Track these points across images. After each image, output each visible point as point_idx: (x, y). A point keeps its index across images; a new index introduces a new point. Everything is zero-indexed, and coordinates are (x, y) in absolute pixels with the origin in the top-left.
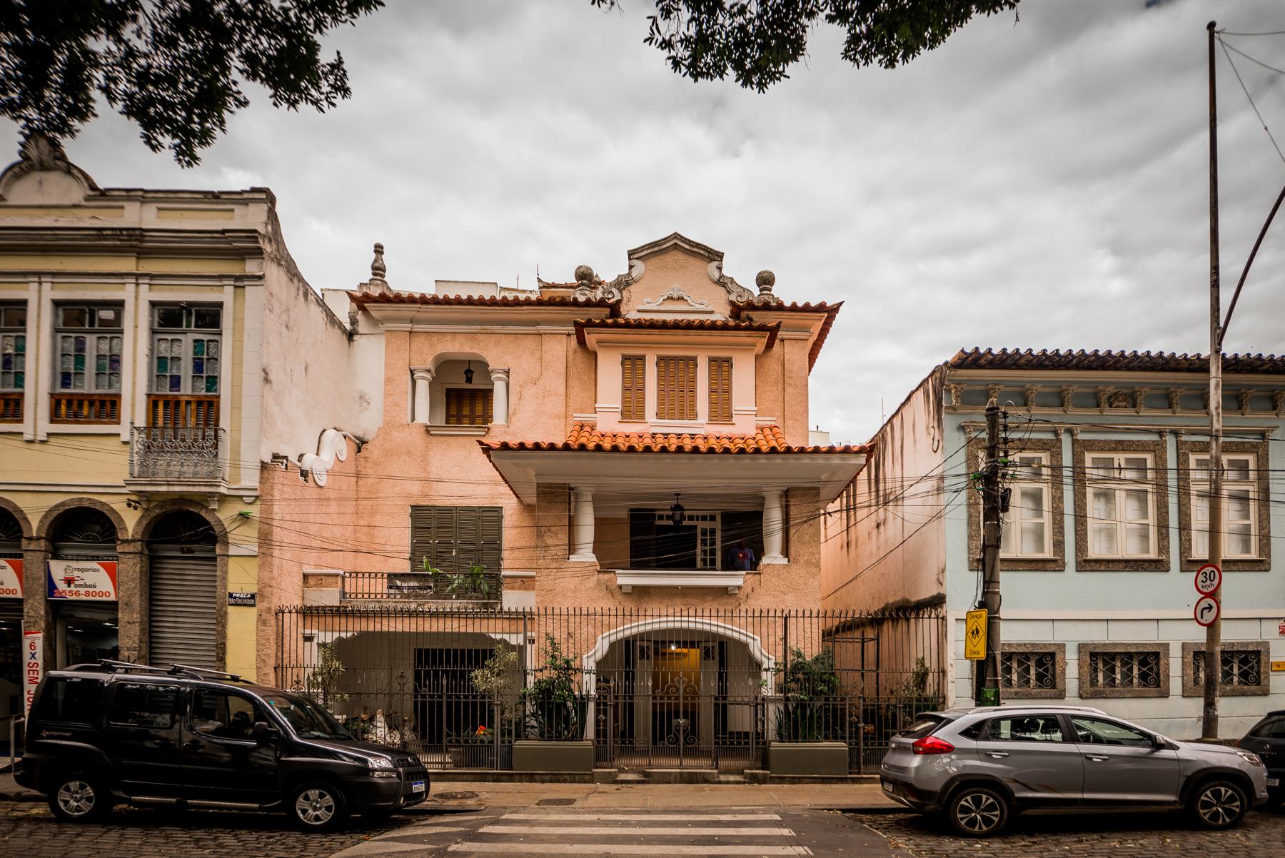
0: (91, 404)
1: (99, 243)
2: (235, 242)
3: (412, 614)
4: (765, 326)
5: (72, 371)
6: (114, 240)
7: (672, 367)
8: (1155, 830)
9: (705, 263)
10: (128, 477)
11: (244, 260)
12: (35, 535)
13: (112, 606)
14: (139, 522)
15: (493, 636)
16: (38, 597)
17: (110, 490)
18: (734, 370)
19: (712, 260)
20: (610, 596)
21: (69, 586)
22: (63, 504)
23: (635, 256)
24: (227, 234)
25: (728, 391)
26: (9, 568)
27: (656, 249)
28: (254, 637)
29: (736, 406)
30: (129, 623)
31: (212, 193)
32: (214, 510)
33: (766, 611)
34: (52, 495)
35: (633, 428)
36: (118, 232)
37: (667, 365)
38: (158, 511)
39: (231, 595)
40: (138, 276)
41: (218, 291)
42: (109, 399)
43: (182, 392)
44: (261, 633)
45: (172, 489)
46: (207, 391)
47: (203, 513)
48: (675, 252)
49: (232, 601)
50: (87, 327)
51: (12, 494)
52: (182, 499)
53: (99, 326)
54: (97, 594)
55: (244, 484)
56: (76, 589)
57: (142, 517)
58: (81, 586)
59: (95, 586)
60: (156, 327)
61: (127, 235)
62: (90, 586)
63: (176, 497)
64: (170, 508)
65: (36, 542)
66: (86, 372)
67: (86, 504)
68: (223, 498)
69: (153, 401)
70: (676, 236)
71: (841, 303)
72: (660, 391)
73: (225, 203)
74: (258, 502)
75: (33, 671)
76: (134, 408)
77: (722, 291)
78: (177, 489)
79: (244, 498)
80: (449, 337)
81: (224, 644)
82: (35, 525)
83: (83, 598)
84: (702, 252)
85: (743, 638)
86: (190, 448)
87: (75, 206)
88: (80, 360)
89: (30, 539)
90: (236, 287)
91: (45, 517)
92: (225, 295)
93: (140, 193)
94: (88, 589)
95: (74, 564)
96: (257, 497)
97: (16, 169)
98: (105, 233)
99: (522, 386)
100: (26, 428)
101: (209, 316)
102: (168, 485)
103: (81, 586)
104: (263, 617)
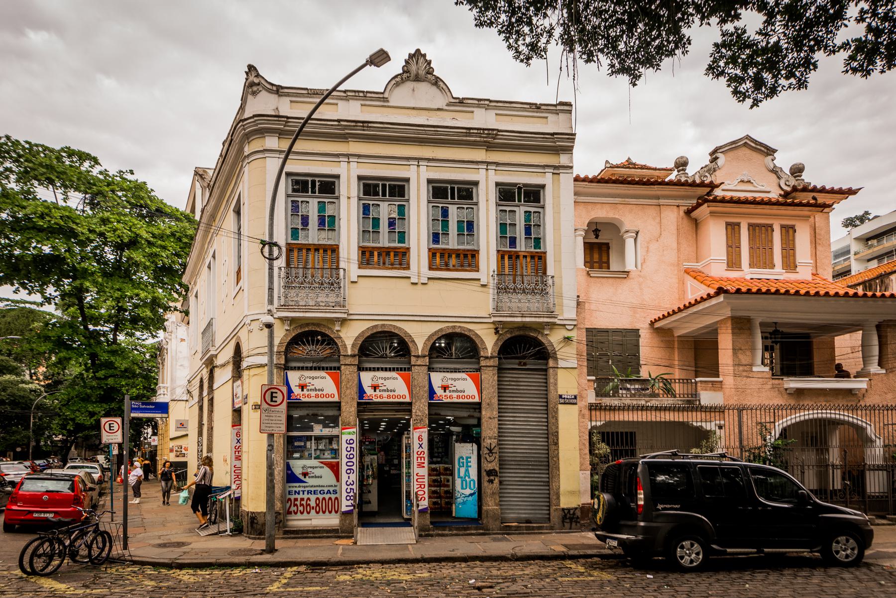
0: (458, 256)
2: (559, 141)
3: (643, 408)
4: (825, 204)
6: (476, 137)
7: (757, 231)
8: (806, 567)
9: (763, 157)
10: (491, 311)
11: (559, 154)
13: (477, 406)
14: (496, 344)
15: (695, 424)
16: (423, 401)
17: (477, 320)
18: (797, 234)
19: (768, 155)
20: (780, 396)
21: (445, 392)
22: (441, 330)
23: (721, 151)
25: (793, 249)
26: (328, 377)
27: (734, 146)
29: (799, 259)
30: (490, 418)
31: (536, 104)
32: (547, 335)
35: (733, 275)
37: (754, 230)
38: (509, 336)
39: (560, 396)
40: (488, 163)
43: (518, 249)
44: (581, 424)
45: (525, 319)
46: (535, 248)
47: (540, 337)
48: (744, 148)
49: (562, 401)
50: (517, 202)
51: (399, 322)
52: (524, 327)
55: (566, 316)
57: (498, 339)
59: (464, 392)
61: (487, 134)
63: (521, 325)
64: (517, 333)
65: (422, 359)
67: (458, 330)
69: (501, 255)
70: (748, 137)
71: (860, 189)
72: (751, 248)
73: (542, 112)
74: (575, 330)
76: (488, 261)
77: (774, 176)
78: (528, 319)
79: (567, 327)
80: (599, 206)
81: (557, 432)
82: (420, 346)
83: (455, 400)
84: (763, 149)
85: (864, 425)
87: (439, 109)
88: (445, 224)
89: (418, 357)
90: (553, 173)
92: (547, 179)
94: (459, 394)
95: (449, 375)
96: (575, 325)
97: (398, 79)
98: (472, 131)
99: (648, 243)
100: (413, 272)
101: (533, 194)
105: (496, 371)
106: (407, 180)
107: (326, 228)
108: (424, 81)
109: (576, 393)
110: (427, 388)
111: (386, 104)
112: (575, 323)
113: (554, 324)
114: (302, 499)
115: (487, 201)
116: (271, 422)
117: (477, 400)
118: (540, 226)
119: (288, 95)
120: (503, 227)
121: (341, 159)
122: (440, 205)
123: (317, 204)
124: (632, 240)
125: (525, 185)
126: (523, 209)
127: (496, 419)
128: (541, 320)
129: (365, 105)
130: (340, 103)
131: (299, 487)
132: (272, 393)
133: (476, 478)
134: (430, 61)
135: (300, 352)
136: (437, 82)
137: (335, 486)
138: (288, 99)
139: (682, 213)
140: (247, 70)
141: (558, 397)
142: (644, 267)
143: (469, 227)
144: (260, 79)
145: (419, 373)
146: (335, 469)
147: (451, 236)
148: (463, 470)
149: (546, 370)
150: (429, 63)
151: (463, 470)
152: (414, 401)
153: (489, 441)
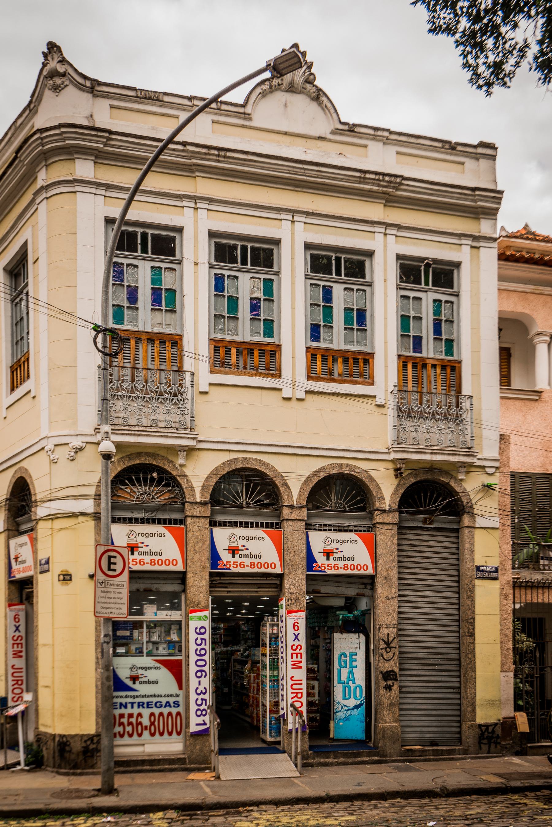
1: (357, 185)
2: (481, 201)
5: (322, 323)
6: (373, 184)
12: (295, 503)
16: (299, 572)
22: (323, 469)
24: (477, 193)
28: (498, 612)
30: (388, 598)
32: (461, 480)
33: (114, 562)
34: (312, 459)
36: (381, 178)
38: (413, 480)
39: (478, 568)
42: (363, 357)
44: (504, 607)
47: (453, 484)
49: (480, 575)
54: (164, 562)
56: (242, 560)
57: (398, 485)
60: (309, 273)
61: (388, 182)
62: (156, 554)
63: (428, 466)
64: (423, 477)
66: (334, 324)
67: (346, 470)
68: (468, 467)
69: (403, 361)
75: (297, 654)
78: (439, 458)
82: (295, 491)
83: (342, 571)
86: (175, 395)
87: (320, 138)
88: (328, 311)
89: (292, 507)
91: (306, 482)
93: (386, 134)
98: (368, 176)
102: (431, 453)
103: (145, 553)
104: (505, 591)
105: (395, 531)
108: (300, 93)
109: (497, 564)
112: (497, 464)
113: (471, 465)
114: (131, 716)
115: (385, 281)
116: (108, 600)
117: (370, 571)
119: (106, 96)
120: (405, 320)
121: (185, 204)
122: (322, 283)
126: (432, 296)
127: (396, 600)
131: (127, 697)
132: (110, 557)
137: (177, 696)
140: (46, 50)
144: (66, 66)
147: (335, 330)
148: (345, 673)
149: (457, 531)
151: (345, 673)
152: (287, 572)
153: (386, 631)
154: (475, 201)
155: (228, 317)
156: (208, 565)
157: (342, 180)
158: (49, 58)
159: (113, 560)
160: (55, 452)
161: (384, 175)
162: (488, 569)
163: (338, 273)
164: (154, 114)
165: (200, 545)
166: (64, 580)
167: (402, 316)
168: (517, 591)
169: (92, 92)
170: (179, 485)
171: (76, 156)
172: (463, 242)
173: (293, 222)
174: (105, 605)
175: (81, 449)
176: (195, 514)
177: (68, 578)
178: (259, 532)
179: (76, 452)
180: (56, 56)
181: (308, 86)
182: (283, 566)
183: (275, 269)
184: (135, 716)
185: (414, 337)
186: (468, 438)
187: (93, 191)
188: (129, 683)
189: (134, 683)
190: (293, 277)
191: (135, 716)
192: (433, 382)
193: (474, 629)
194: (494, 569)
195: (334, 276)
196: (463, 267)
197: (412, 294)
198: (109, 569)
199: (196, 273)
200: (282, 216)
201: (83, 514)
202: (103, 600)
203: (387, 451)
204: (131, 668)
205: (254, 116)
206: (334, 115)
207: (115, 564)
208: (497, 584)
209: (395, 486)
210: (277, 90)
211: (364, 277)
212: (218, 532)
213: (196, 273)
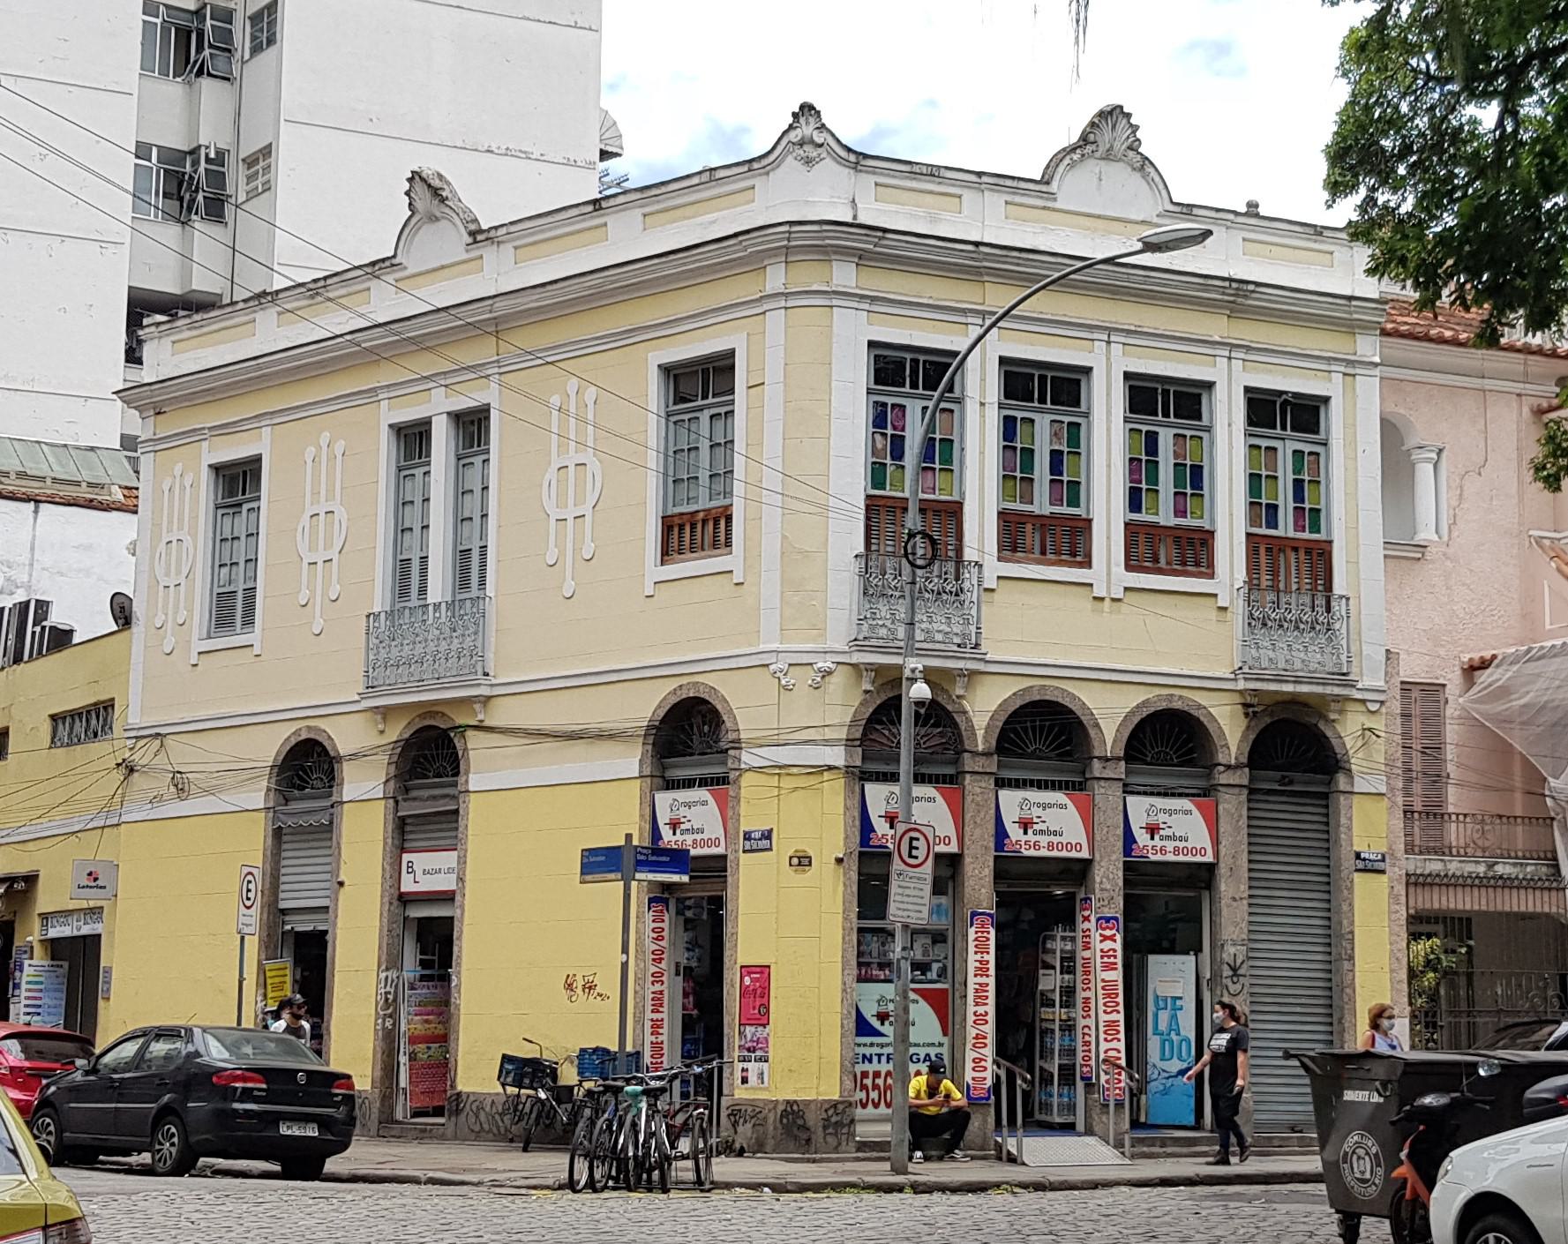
2: (1357, 313)
6: (1217, 293)
16: (1114, 857)
22: (1145, 703)
24: (1354, 303)
30: (1234, 899)
32: (1334, 721)
39: (1358, 856)
41: (1324, 378)
44: (1394, 916)
47: (1322, 725)
49: (1360, 865)
52: (1294, 701)
53: (924, 389)
56: (1038, 838)
57: (1248, 728)
58: (1168, 838)
61: (1237, 289)
67: (1177, 705)
78: (1305, 689)
94: (1177, 843)
96: (1382, 703)
102: (1295, 682)
103: (1168, 838)
105: (1244, 797)
106: (1087, 371)
107: (937, 466)
108: (1120, 160)
109: (1384, 850)
110: (1120, 831)
111: (1050, 204)
112: (1382, 697)
113: (1348, 699)
114: (877, 1074)
115: (1230, 425)
116: (906, 899)
117: (1209, 858)
118: (1319, 482)
119: (873, 171)
120: (1254, 479)
121: (970, 320)
122: (1145, 428)
123: (854, 374)
124: (1431, 467)
125: (1296, 395)
126: (1292, 446)
127: (1245, 902)
128: (1329, 690)
129: (1011, 203)
130: (968, 195)
131: (872, 1045)
132: (912, 839)
133: (1192, 1036)
134: (1137, 127)
135: (885, 741)
136: (1144, 165)
137: (941, 1045)
138: (873, 179)
139: (1526, 410)
140: (797, 110)
141: (1353, 856)
142: (1455, 534)
143: (1193, 478)
144: (825, 134)
145: (1106, 796)
146: (943, 1005)
147: (1161, 496)
148: (1164, 1017)
149: (1325, 796)
150: (1135, 128)
151: (1164, 1017)
152: (1097, 857)
153: (1232, 950)
154: (1350, 313)
155: (1022, 478)
156: (992, 845)
157: (1176, 287)
158: (802, 120)
159: (915, 843)
160: (789, 674)
161: (1231, 280)
162: (1372, 857)
163: (1166, 415)
164: (931, 192)
165: (982, 814)
166: (800, 864)
167: (1251, 475)
168: (1412, 889)
169: (855, 168)
170: (955, 725)
171: (833, 257)
172: (1333, 368)
173: (1109, 342)
174: (901, 906)
175: (830, 673)
176: (977, 769)
177: (806, 861)
178: (1059, 797)
179: (823, 677)
180: (811, 120)
181: (1131, 154)
182: (1092, 850)
183: (1083, 408)
184: (883, 1075)
185: (1268, 505)
186: (1344, 658)
187: (855, 305)
188: (876, 1023)
189: (882, 1024)
190: (1109, 421)
191: (883, 1075)
192: (1293, 572)
193: (1353, 949)
194: (1380, 857)
195: (1160, 418)
196: (1333, 402)
197: (1264, 443)
198: (910, 856)
199: (983, 416)
200: (1095, 336)
201: (830, 768)
202: (898, 898)
203: (1232, 676)
204: (879, 1001)
205: (1059, 196)
206: (1164, 192)
207: (917, 848)
208: (1384, 878)
209: (1243, 728)
210: (1089, 157)
211: (1199, 418)
212: (1005, 795)
213: (983, 416)
